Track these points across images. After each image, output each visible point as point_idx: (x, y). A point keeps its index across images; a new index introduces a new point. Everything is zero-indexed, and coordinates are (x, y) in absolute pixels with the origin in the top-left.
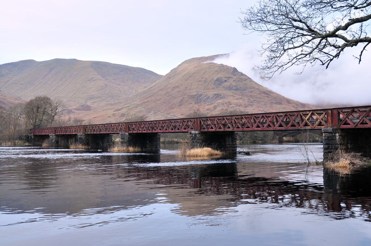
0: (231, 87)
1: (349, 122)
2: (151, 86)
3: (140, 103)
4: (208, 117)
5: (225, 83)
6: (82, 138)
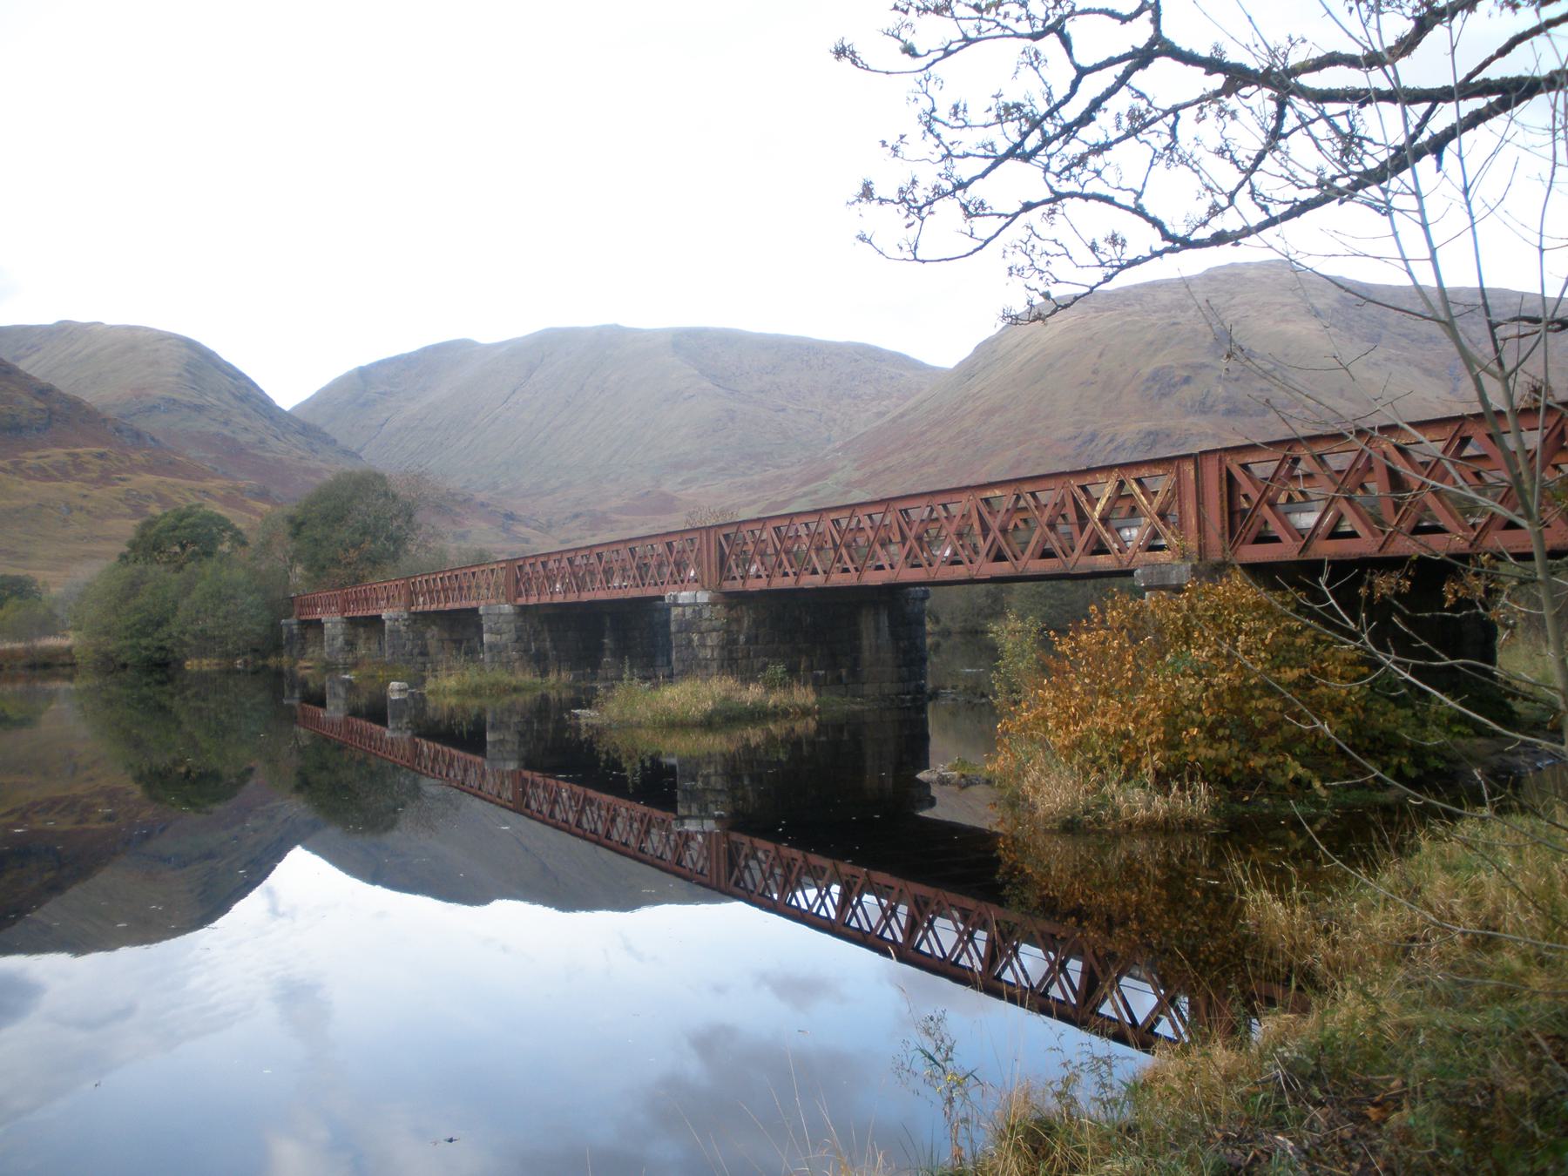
0: (1209, 402)
1: (1275, 527)
2: (900, 410)
3: (857, 475)
4: (744, 522)
5: (1185, 387)
6: (399, 631)
